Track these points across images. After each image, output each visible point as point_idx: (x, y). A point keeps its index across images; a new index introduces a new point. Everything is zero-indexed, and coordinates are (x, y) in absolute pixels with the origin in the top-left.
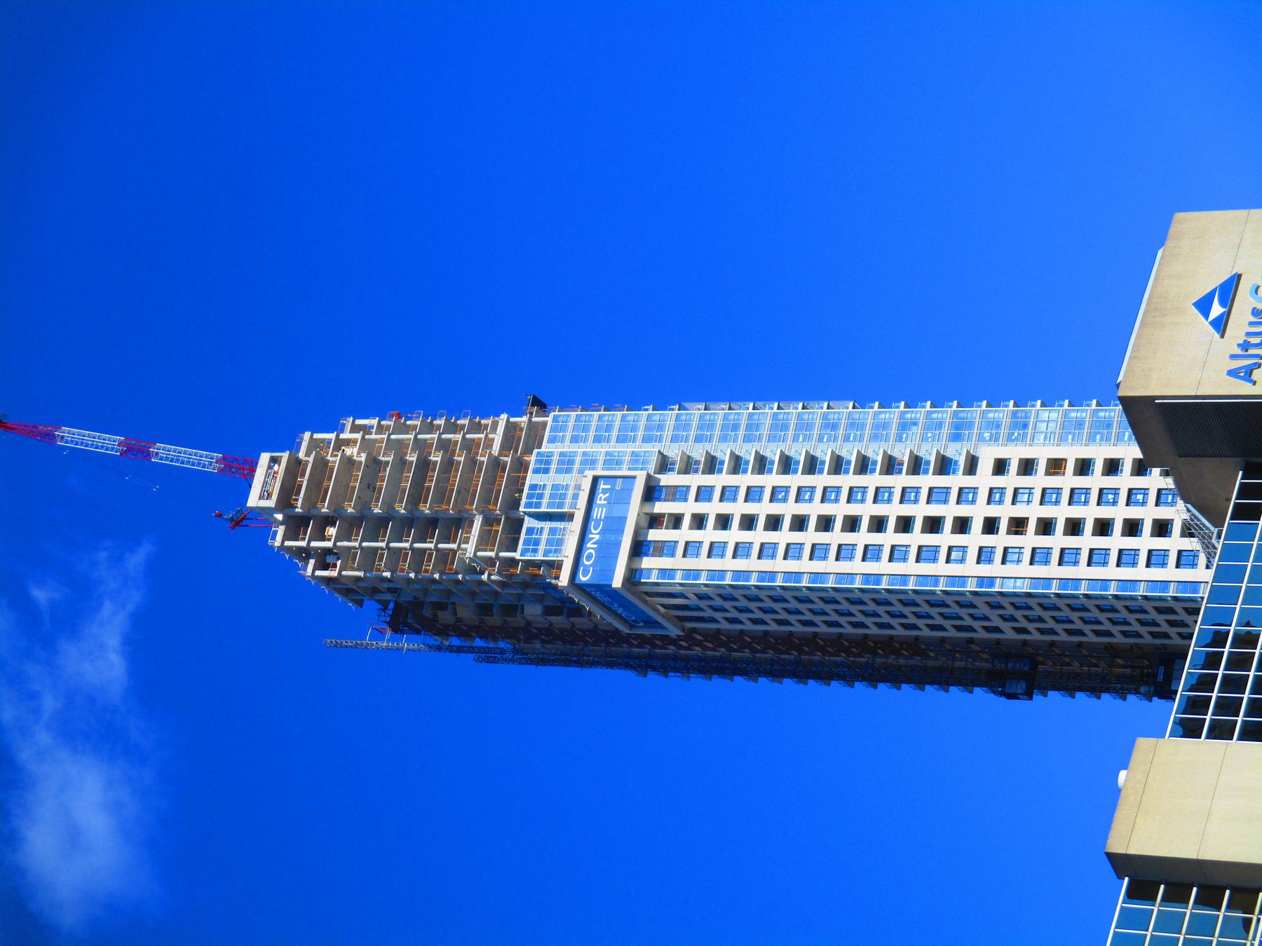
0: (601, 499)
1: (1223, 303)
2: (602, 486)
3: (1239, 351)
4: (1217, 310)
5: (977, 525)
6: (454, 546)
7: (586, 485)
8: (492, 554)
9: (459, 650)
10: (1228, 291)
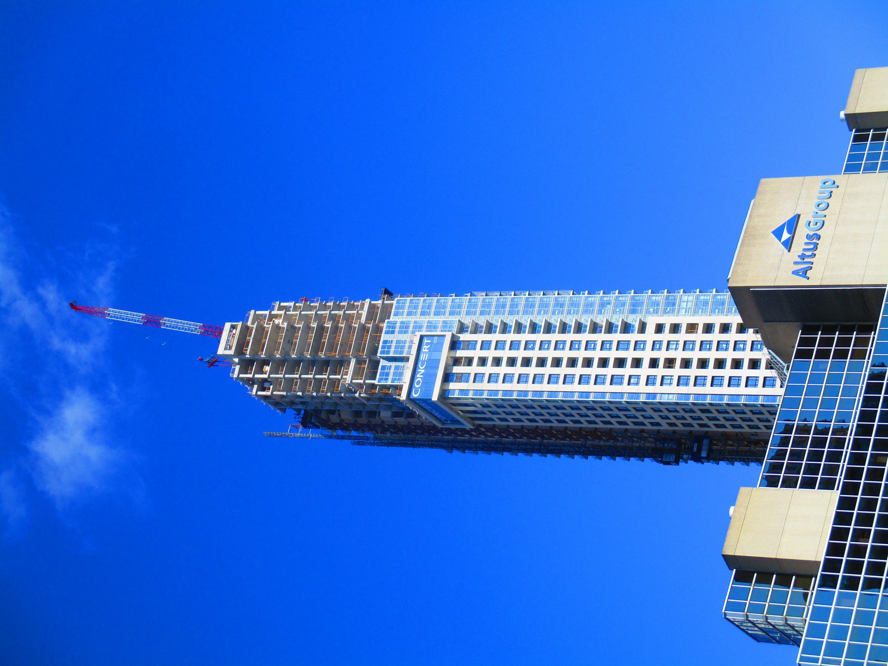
0: (425, 348)
1: (789, 232)
2: (426, 341)
3: (799, 260)
4: (786, 236)
5: (646, 363)
6: (339, 377)
7: (416, 340)
8: (361, 381)
9: (343, 438)
10: (793, 224)
